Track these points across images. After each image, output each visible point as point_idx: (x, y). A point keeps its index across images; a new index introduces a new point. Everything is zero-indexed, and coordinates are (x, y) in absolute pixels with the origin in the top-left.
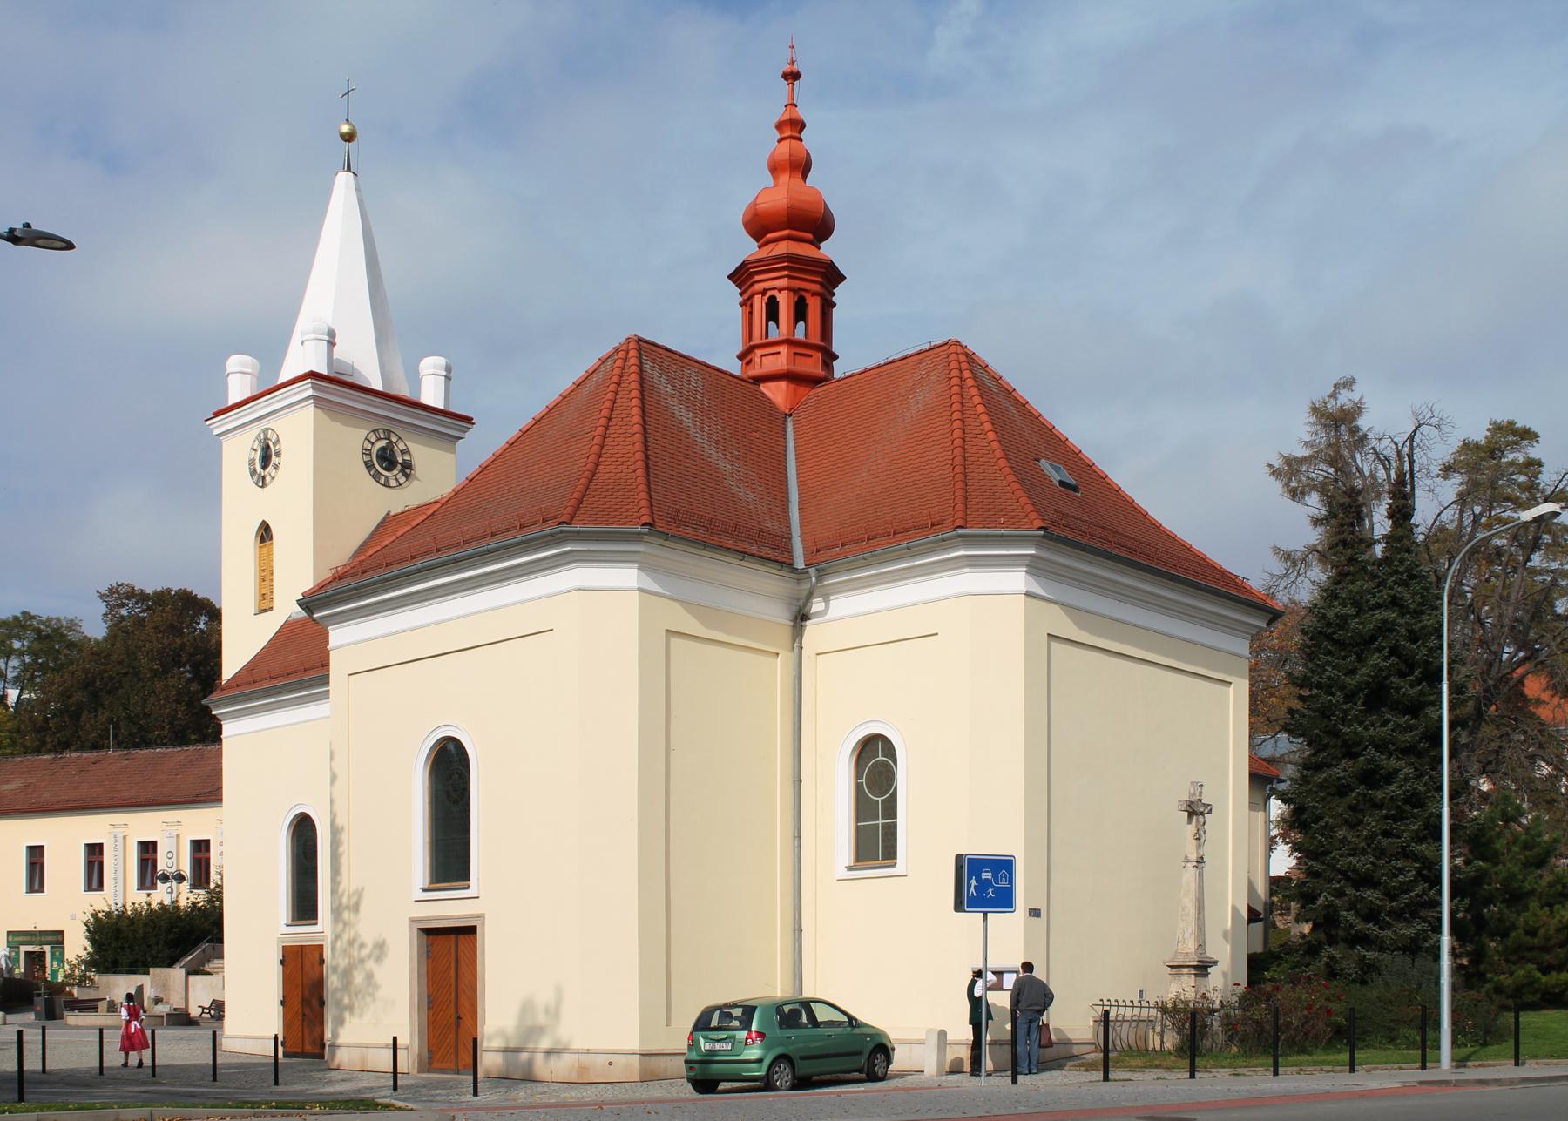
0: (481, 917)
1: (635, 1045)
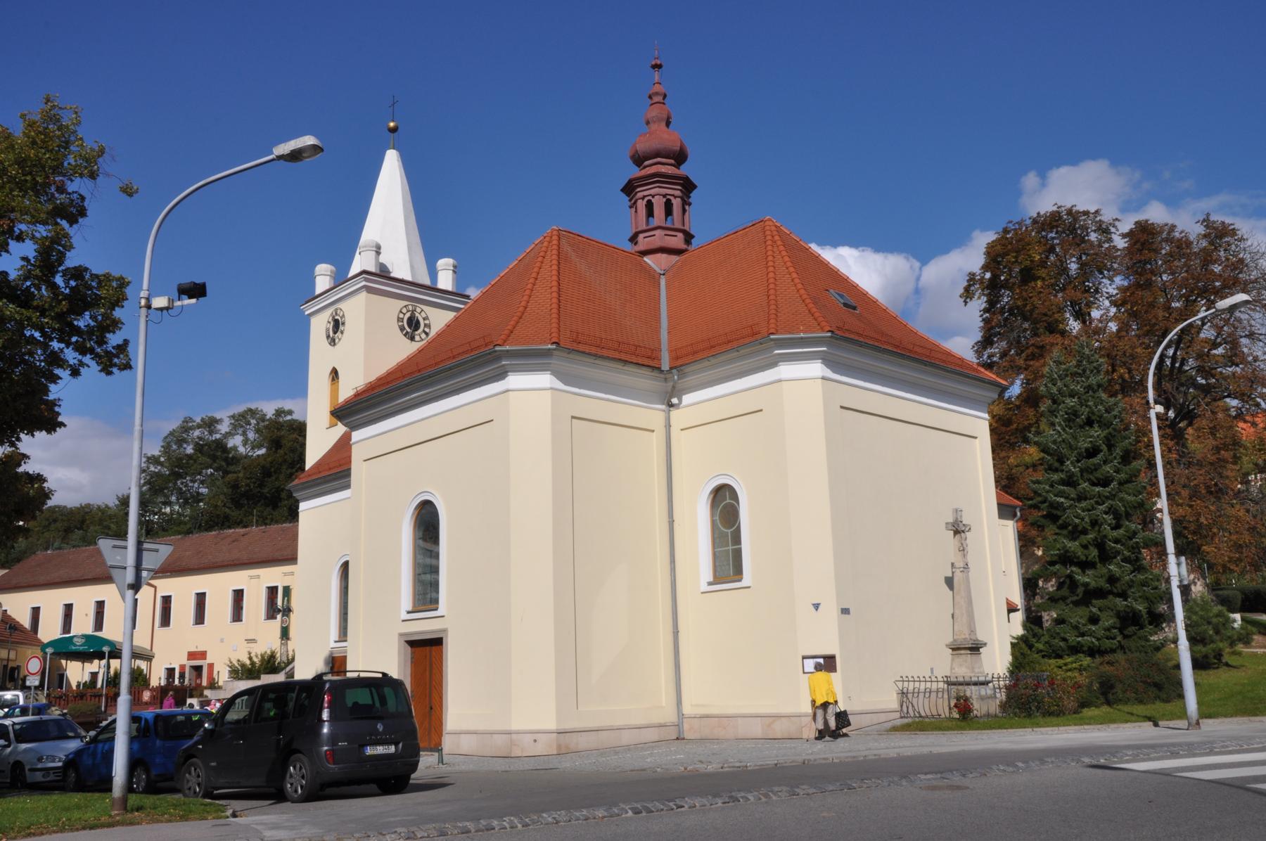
0: (445, 631)
1: (552, 726)
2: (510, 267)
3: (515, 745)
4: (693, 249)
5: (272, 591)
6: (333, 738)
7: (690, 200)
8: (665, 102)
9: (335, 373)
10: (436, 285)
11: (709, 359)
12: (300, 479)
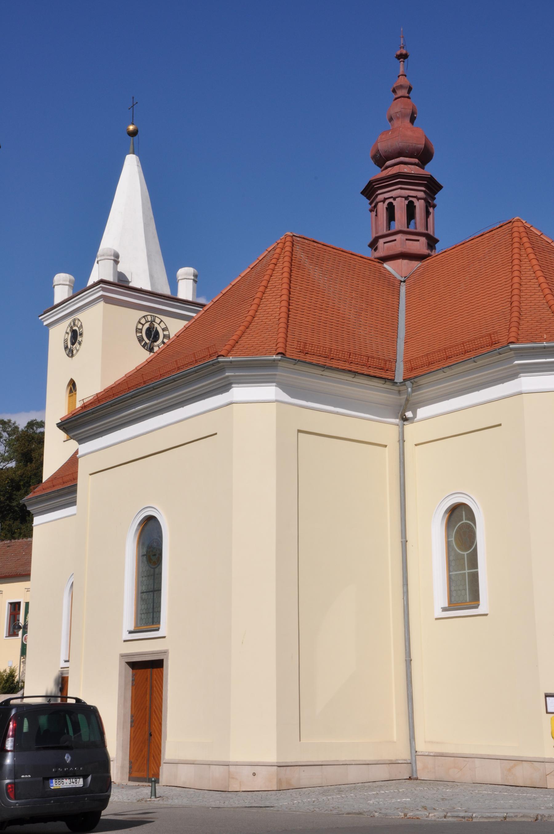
0: (166, 652)
1: (272, 758)
2: (242, 275)
3: (233, 778)
4: (437, 254)
5: (15, 607)
6: (16, 771)
7: (435, 202)
8: (410, 95)
9: (72, 385)
10: (176, 295)
11: (445, 370)
12: (34, 493)
